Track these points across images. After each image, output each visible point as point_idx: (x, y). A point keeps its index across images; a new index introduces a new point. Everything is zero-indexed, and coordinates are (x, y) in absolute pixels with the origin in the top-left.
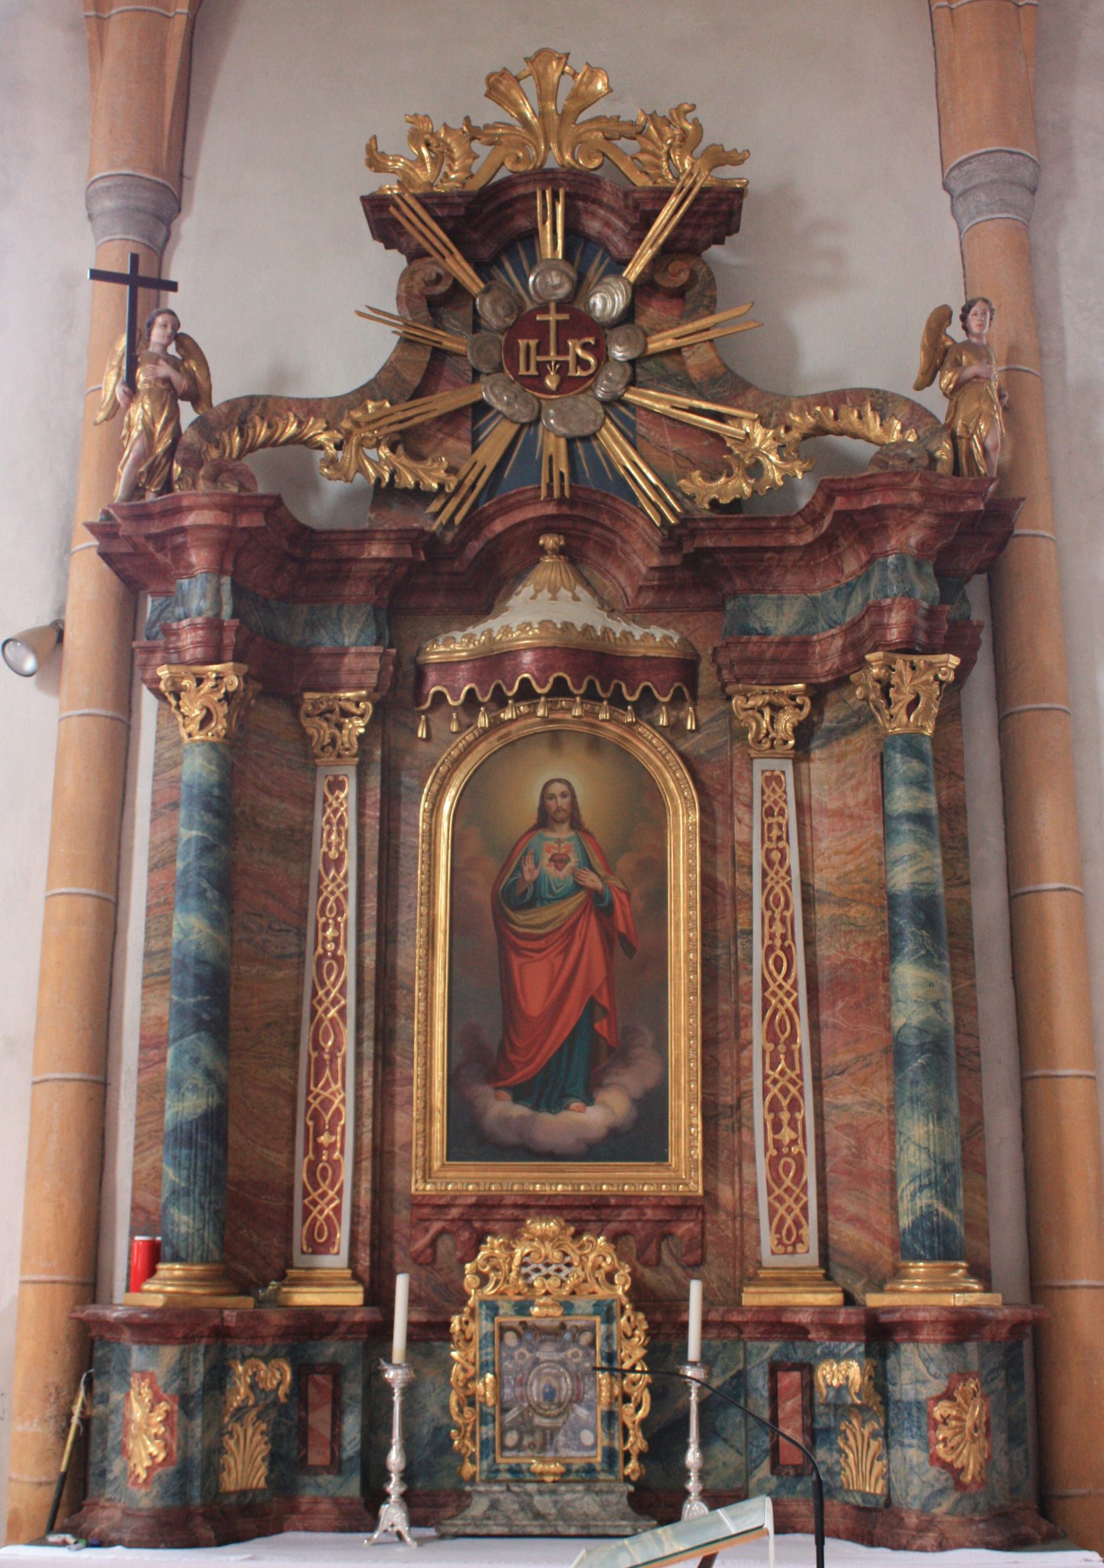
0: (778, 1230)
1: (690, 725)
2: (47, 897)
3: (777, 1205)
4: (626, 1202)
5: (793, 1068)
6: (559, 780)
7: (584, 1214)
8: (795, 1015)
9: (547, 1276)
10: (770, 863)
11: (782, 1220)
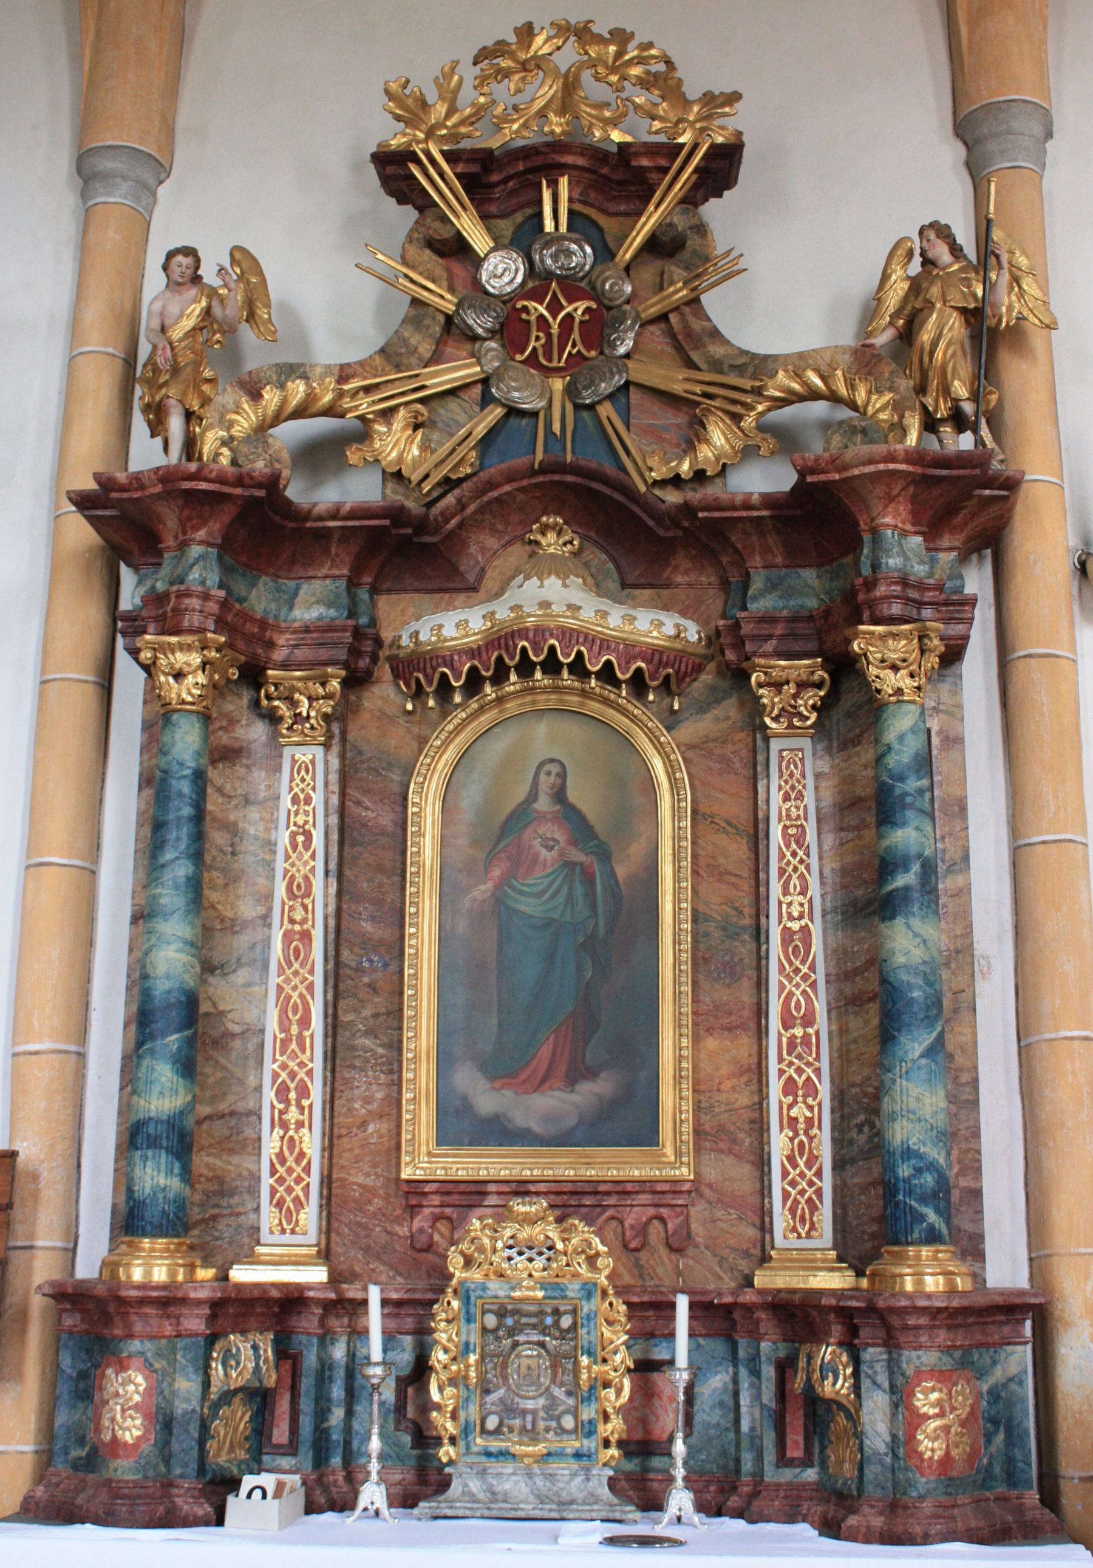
0: (793, 1211)
1: (676, 707)
2: (28, 867)
3: (790, 1189)
4: (623, 1190)
5: (303, 1051)
6: (552, 761)
7: (571, 1201)
8: (309, 997)
9: (530, 1260)
10: (295, 847)
11: (796, 1202)
